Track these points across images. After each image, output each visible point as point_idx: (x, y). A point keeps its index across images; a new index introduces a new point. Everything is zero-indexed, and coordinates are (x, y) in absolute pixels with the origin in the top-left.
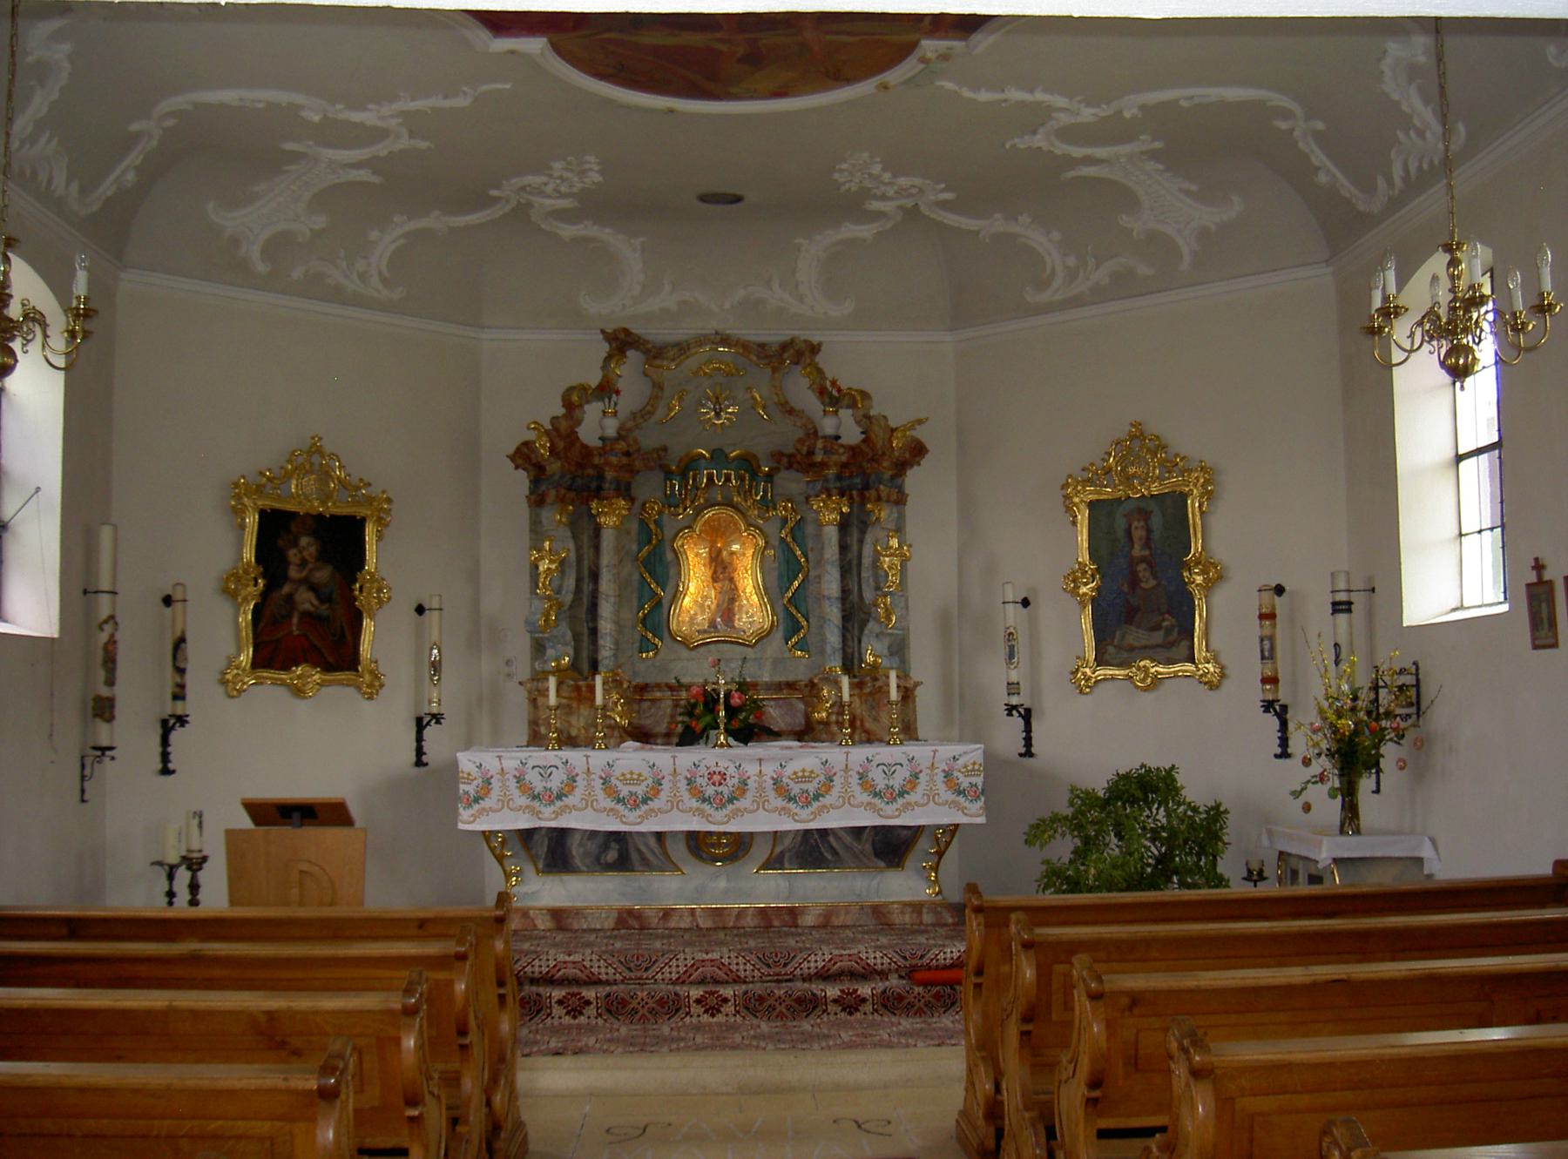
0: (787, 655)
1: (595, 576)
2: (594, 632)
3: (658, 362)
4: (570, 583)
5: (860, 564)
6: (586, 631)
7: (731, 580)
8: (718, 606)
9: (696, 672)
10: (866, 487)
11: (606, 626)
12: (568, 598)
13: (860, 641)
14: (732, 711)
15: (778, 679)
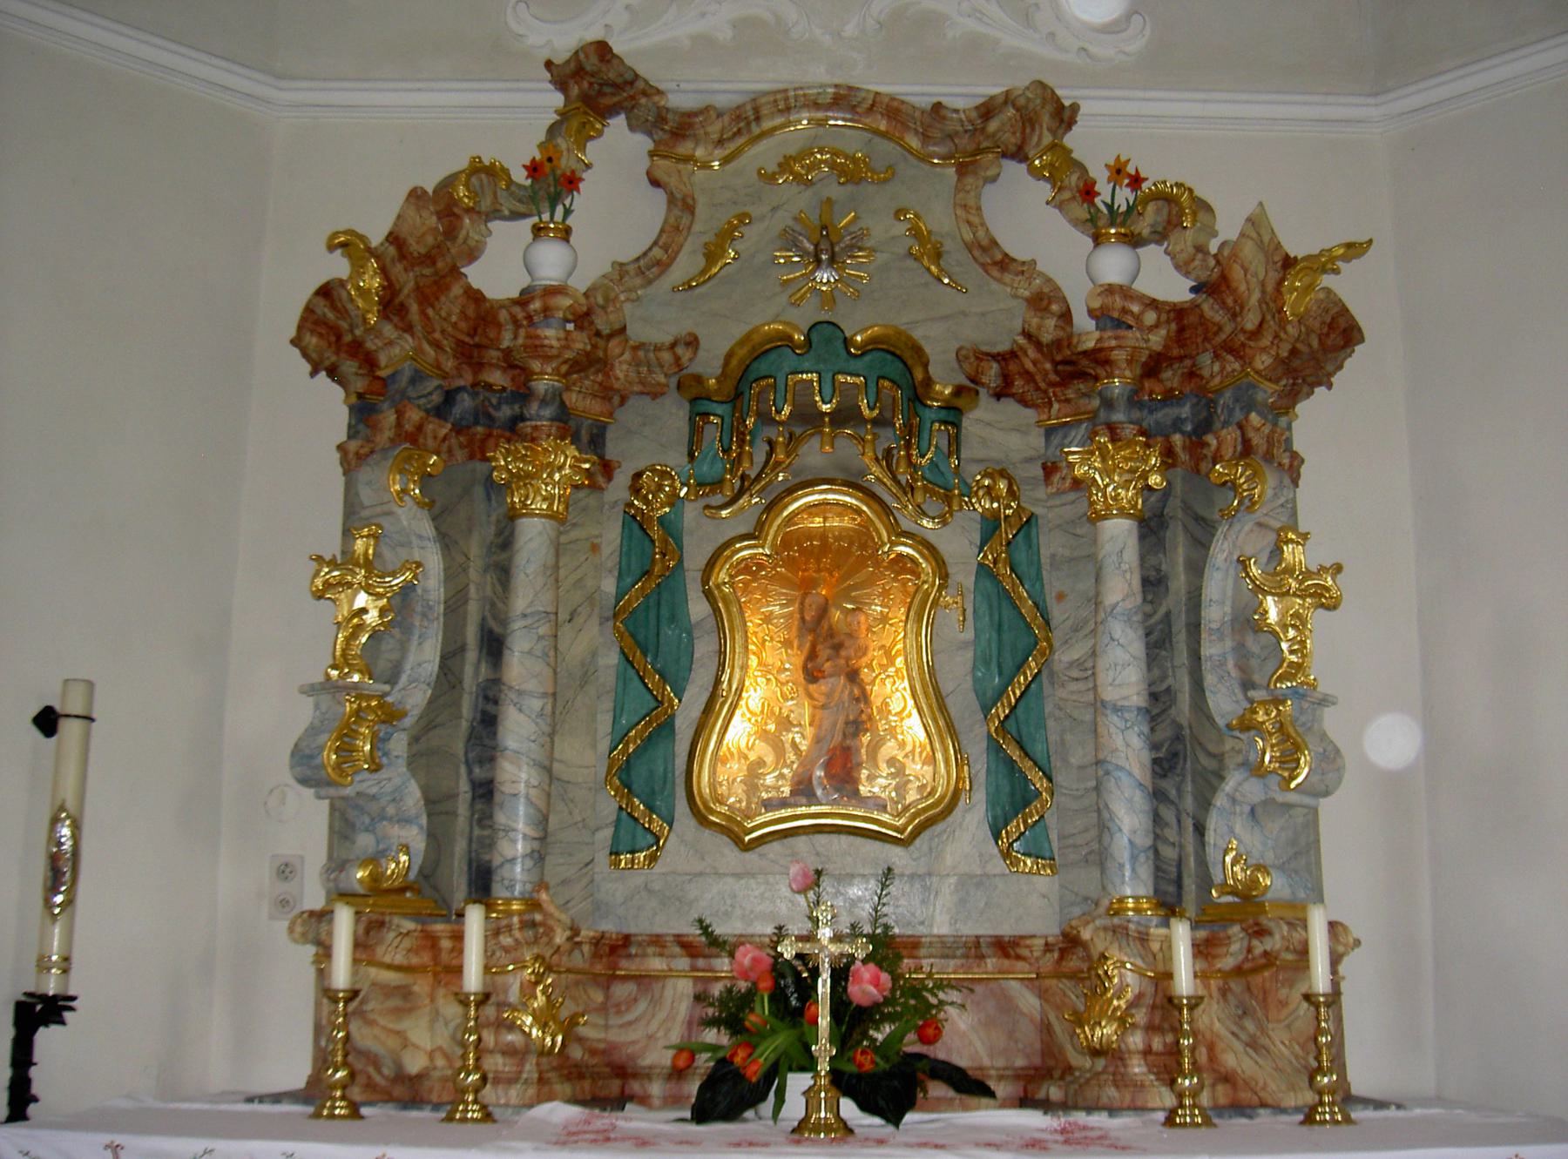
0: (999, 865)
1: (494, 646)
2: (485, 791)
3: (684, 148)
4: (425, 656)
5: (1195, 628)
6: (464, 786)
7: (853, 676)
8: (818, 740)
9: (759, 906)
10: (1205, 426)
11: (517, 777)
12: (414, 697)
13: (1200, 830)
14: (852, 1019)
15: (969, 929)
